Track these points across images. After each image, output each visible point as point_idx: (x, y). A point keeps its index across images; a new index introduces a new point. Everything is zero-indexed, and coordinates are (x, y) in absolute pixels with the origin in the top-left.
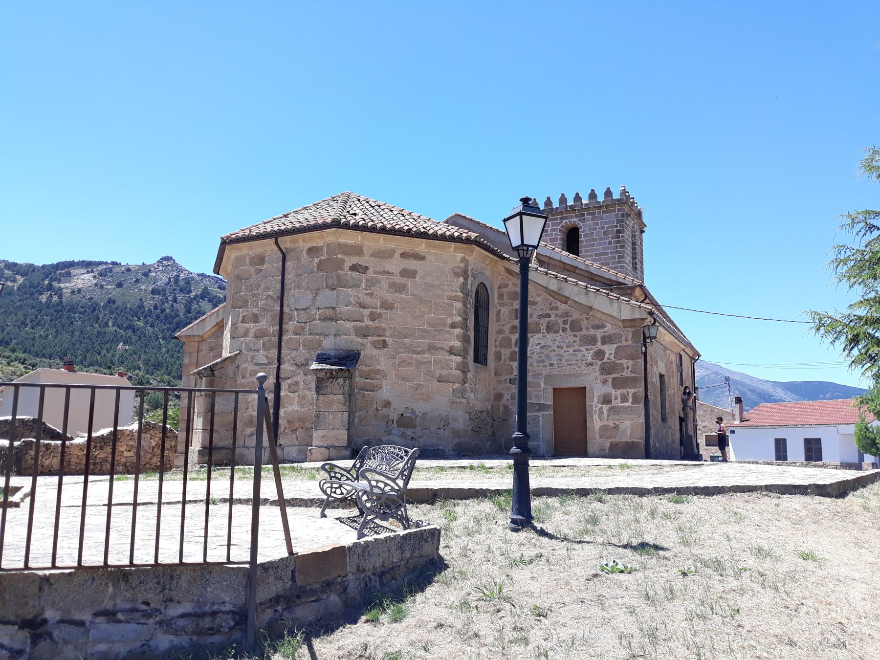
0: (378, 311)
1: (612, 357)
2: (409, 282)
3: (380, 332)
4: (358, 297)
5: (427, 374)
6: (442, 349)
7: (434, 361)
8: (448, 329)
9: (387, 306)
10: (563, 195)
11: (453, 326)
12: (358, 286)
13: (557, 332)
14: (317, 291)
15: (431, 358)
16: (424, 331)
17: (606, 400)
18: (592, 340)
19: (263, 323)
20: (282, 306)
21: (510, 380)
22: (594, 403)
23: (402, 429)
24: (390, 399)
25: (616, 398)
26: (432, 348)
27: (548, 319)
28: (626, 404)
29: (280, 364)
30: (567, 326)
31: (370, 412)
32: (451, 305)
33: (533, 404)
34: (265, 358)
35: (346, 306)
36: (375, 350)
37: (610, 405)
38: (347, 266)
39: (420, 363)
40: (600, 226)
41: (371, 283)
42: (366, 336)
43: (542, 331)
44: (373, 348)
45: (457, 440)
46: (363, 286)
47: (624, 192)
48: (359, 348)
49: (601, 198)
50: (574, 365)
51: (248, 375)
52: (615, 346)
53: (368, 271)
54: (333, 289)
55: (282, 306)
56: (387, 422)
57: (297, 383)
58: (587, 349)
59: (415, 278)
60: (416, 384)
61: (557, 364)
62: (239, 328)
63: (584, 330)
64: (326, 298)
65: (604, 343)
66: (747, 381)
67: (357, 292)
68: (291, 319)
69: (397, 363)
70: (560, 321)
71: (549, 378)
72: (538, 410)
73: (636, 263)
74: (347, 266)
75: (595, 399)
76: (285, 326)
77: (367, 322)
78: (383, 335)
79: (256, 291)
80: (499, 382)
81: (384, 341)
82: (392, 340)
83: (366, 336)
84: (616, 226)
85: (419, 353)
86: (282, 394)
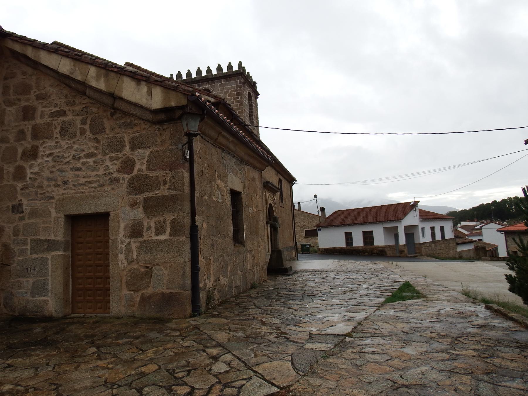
1: (144, 167)
18: (118, 145)
25: (149, 228)
27: (62, 119)
28: (163, 237)
30: (87, 127)
33: (40, 240)
37: (141, 239)
40: (225, 90)
43: (55, 135)
47: (240, 64)
49: (225, 70)
50: (94, 182)
52: (148, 152)
58: (111, 159)
63: (107, 131)
65: (133, 147)
66: (451, 260)
70: (78, 119)
73: (253, 119)
84: (236, 90)
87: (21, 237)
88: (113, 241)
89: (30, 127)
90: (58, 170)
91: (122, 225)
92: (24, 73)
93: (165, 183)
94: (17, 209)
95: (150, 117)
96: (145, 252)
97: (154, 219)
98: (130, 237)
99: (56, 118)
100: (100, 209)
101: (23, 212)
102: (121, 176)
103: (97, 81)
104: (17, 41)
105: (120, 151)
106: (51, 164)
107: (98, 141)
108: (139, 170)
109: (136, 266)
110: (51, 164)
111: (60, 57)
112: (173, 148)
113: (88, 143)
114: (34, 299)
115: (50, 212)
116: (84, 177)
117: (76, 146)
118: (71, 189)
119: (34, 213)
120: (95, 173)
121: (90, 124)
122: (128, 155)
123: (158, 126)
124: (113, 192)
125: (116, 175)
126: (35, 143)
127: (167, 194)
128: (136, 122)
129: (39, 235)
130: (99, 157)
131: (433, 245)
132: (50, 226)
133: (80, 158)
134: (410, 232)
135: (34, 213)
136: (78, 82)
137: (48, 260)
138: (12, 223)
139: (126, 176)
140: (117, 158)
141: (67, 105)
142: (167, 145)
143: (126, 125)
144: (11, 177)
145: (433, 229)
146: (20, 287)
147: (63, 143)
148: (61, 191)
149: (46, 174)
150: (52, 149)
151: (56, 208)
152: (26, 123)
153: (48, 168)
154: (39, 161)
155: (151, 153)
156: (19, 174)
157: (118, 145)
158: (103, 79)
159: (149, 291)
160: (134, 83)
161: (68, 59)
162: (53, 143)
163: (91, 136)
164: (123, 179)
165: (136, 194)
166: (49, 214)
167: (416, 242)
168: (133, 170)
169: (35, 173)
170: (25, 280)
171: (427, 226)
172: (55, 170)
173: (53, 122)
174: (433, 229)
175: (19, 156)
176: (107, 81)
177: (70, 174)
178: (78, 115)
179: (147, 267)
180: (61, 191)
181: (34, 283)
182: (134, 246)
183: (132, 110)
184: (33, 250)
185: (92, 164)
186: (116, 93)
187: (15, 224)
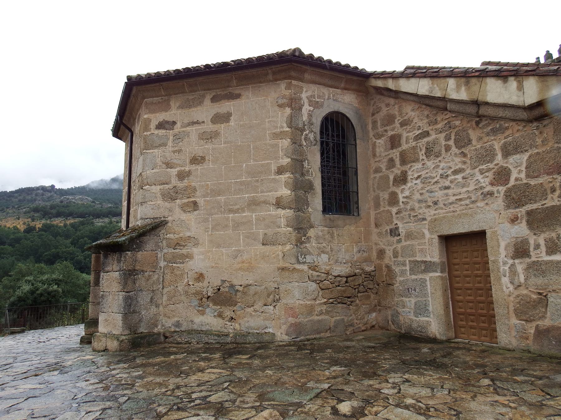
1: (523, 175)
2: (222, 128)
3: (191, 191)
5: (248, 237)
6: (265, 202)
7: (256, 219)
8: (273, 177)
11: (280, 171)
15: (252, 216)
16: (242, 183)
18: (489, 155)
23: (219, 307)
24: (204, 272)
26: (254, 204)
27: (426, 140)
30: (451, 143)
31: (179, 288)
32: (277, 145)
35: (153, 169)
36: (185, 215)
37: (528, 260)
38: (153, 125)
39: (237, 225)
42: (174, 200)
43: (421, 158)
44: (182, 212)
45: (291, 320)
46: (170, 143)
48: (166, 214)
53: (175, 127)
56: (201, 299)
60: (235, 250)
63: (474, 142)
67: (164, 152)
69: (210, 226)
72: (424, 270)
77: (175, 182)
78: (193, 196)
81: (195, 203)
82: (205, 201)
83: (173, 199)
85: (236, 211)
87: (400, 259)
88: (494, 262)
91: (503, 244)
93: (553, 190)
94: (394, 232)
95: (524, 115)
96: (535, 275)
98: (513, 258)
99: (420, 141)
100: (475, 228)
101: (399, 235)
102: (495, 189)
105: (491, 161)
108: (517, 179)
109: (525, 292)
113: (454, 158)
114: (418, 319)
115: (424, 233)
116: (454, 195)
117: (442, 165)
118: (442, 209)
120: (465, 189)
122: (501, 164)
123: (535, 124)
124: (487, 208)
125: (489, 188)
128: (507, 125)
133: (447, 176)
135: (409, 236)
136: (439, 99)
137: (426, 281)
138: (391, 246)
139: (501, 188)
140: (489, 170)
141: (430, 125)
142: (550, 144)
143: (494, 131)
144: (387, 203)
146: (404, 307)
148: (433, 212)
149: (417, 196)
151: (429, 229)
154: (409, 185)
155: (530, 157)
156: (393, 200)
157: (489, 155)
158: (463, 88)
164: (498, 192)
165: (516, 208)
166: (423, 235)
170: (407, 299)
176: (468, 88)
177: (439, 194)
178: (441, 132)
179: (540, 294)
180: (433, 212)
183: (501, 113)
184: (412, 271)
185: (460, 180)
186: (481, 99)
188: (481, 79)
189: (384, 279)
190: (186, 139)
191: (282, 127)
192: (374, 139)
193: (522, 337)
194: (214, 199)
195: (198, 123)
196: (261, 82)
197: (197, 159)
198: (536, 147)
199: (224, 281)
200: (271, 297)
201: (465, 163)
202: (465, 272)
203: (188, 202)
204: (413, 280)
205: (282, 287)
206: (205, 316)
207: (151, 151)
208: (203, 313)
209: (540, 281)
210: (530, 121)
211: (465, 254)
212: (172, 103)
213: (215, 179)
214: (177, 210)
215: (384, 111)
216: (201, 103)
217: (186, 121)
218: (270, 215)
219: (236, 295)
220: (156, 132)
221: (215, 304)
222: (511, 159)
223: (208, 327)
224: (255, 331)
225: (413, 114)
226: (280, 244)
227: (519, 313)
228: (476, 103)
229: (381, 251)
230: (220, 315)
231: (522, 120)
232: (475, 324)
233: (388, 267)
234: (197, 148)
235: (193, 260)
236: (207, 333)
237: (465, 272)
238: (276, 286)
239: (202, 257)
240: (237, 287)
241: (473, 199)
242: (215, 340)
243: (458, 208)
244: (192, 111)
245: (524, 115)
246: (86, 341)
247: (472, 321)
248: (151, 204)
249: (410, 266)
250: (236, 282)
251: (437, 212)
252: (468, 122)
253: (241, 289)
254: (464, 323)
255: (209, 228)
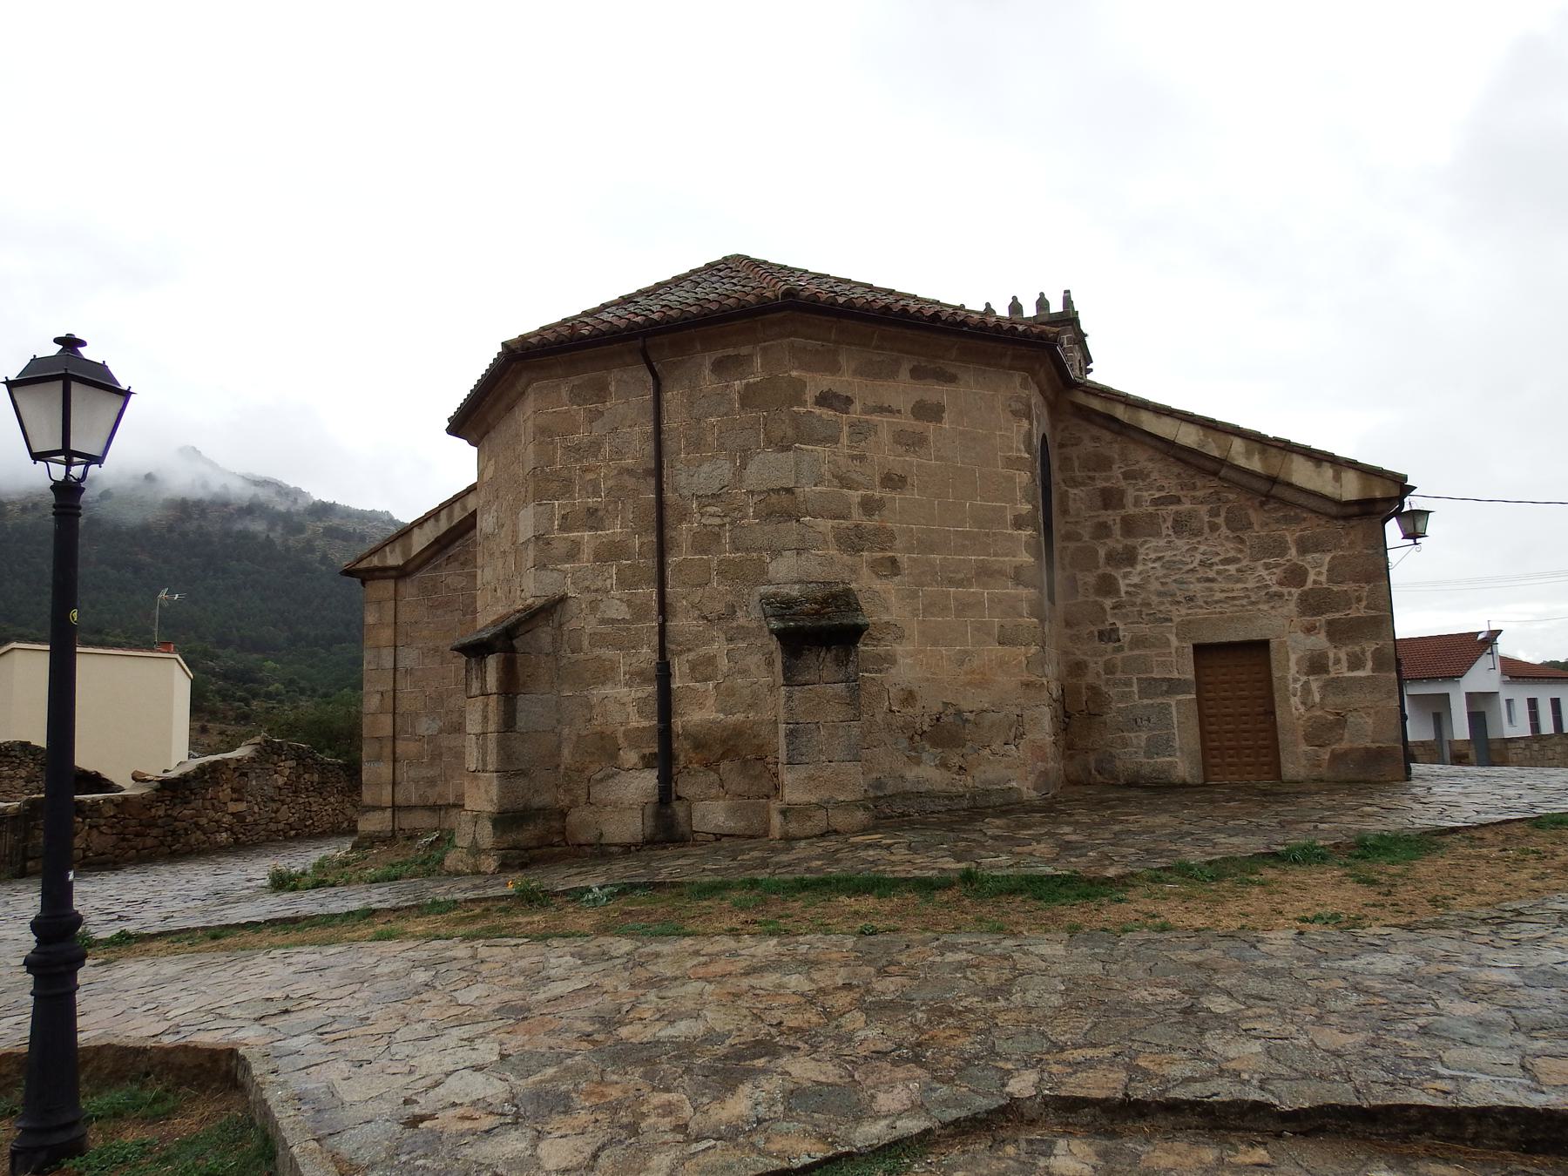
0: (877, 495)
1: (1323, 578)
3: (884, 538)
4: (835, 463)
5: (978, 630)
6: (1001, 573)
7: (991, 600)
8: (1009, 532)
9: (893, 481)
10: (1015, 298)
12: (835, 440)
13: (1199, 533)
14: (746, 455)
16: (965, 535)
17: (1316, 665)
18: (1280, 548)
19: (615, 530)
20: (660, 490)
21: (1101, 634)
22: (1289, 670)
23: (940, 750)
24: (916, 689)
26: (985, 573)
27: (1174, 508)
29: (665, 620)
30: (1220, 520)
32: (1011, 479)
33: (1154, 679)
34: (624, 608)
35: (816, 485)
36: (878, 582)
37: (1325, 676)
39: (963, 607)
41: (860, 431)
42: (858, 551)
43: (1164, 532)
44: (874, 576)
46: (844, 440)
48: (846, 576)
50: (1243, 598)
51: (586, 643)
52: (1327, 558)
53: (852, 409)
54: (788, 449)
55: (660, 490)
57: (710, 660)
58: (1267, 567)
59: (941, 422)
61: (1202, 596)
62: (555, 544)
63: (1256, 527)
64: (768, 469)
68: (684, 516)
70: (1203, 510)
71: (1185, 628)
72: (1167, 692)
74: (810, 395)
75: (1292, 664)
76: (669, 533)
78: (890, 547)
79: (592, 461)
80: (1075, 639)
81: (893, 561)
83: (856, 550)
85: (959, 583)
86: (676, 684)
87: (1118, 675)
88: (1279, 678)
89: (1118, 520)
90: (1175, 581)
91: (1293, 658)
92: (1096, 439)
93: (1359, 600)
94: (1109, 635)
95: (1334, 510)
96: (1334, 693)
97: (1344, 649)
98: (1308, 674)
99: (1162, 507)
100: (1255, 636)
101: (1119, 640)
102: (1285, 590)
103: (1247, 459)
104: (1094, 394)
105: (1281, 555)
106: (1161, 572)
107: (1242, 541)
108: (1315, 582)
109: (1319, 713)
110: (1161, 572)
111: (1178, 422)
112: (1370, 552)
113: (1224, 542)
114: (1152, 761)
115: (1168, 639)
116: (1222, 591)
117: (1202, 548)
118: (1201, 607)
119: (1138, 642)
120: (1240, 586)
121: (1226, 518)
122: (1295, 560)
123: (1342, 522)
124: (1273, 612)
125: (1275, 588)
126: (1129, 542)
127: (1365, 615)
128: (1305, 515)
129: (1152, 672)
130: (1245, 563)
131: (1536, 747)
132: (1170, 659)
133: (1212, 564)
134: (1480, 706)
135: (1138, 642)
137: (1170, 706)
138: (1101, 656)
139: (1293, 590)
140: (1277, 566)
141: (1182, 489)
142: (1359, 549)
143: (1287, 519)
144: (1092, 591)
145: (1533, 703)
146: (1126, 745)
147: (1179, 543)
148: (1184, 611)
149: (1155, 586)
150: (1162, 551)
151: (1177, 635)
152: (1110, 512)
153: (1157, 578)
154: (1139, 568)
155: (1333, 558)
156: (1107, 586)
157: (1280, 548)
158: (1257, 457)
159: (1344, 745)
160: (1310, 463)
161: (1192, 426)
162: (1162, 543)
163: (1228, 533)
164: (1290, 594)
165: (1313, 615)
166: (1168, 643)
167: (1490, 736)
168: (1306, 582)
169: (1135, 586)
170: (1132, 735)
171: (1521, 695)
172: (1168, 580)
173: (1159, 512)
174: (1533, 703)
175: (1102, 560)
176: (1264, 459)
177: (1197, 588)
178: (1202, 503)
179: (1338, 714)
180: (1184, 611)
181: (1148, 739)
182: (1315, 686)
183: (1302, 500)
184: (1143, 693)
185: (1234, 572)
186: (1282, 476)
187: (1107, 658)
188: (1284, 452)
189: (1084, 707)
190: (872, 438)
191: (1019, 450)
192: (1062, 485)
193: (1314, 765)
194: (925, 557)
195: (890, 412)
196: (988, 365)
197: (892, 480)
198: (1342, 548)
199: (946, 704)
200: (1014, 729)
201: (1241, 551)
202: (1223, 694)
203: (882, 558)
204: (1146, 706)
205: (1027, 714)
206: (922, 766)
207: (810, 447)
208: (918, 762)
209: (1339, 700)
210: (1336, 518)
211: (1224, 670)
212: (842, 360)
213: (923, 521)
214: (865, 571)
215: (1088, 446)
216: (893, 374)
217: (871, 402)
218: (1006, 593)
219: (964, 727)
220: (817, 411)
221: (935, 744)
222: (1309, 557)
223: (927, 786)
224: (995, 787)
225: (1150, 465)
226: (1021, 644)
227: (1309, 739)
228: (1273, 480)
229: (1077, 664)
230: (944, 765)
231: (1326, 514)
232: (1235, 760)
233: (1093, 689)
234: (892, 458)
235: (897, 666)
236: (930, 795)
237: (1223, 694)
238: (1019, 713)
239: (909, 661)
240: (967, 715)
241: (1253, 599)
242: (946, 805)
243: (1228, 609)
244: (881, 385)
245: (1334, 510)
246: (517, 862)
247: (1248, 756)
248: (817, 555)
249: (1139, 687)
250: (965, 706)
251: (1189, 612)
252: (1249, 499)
253: (971, 717)
254: (1218, 760)
255: (918, 609)
